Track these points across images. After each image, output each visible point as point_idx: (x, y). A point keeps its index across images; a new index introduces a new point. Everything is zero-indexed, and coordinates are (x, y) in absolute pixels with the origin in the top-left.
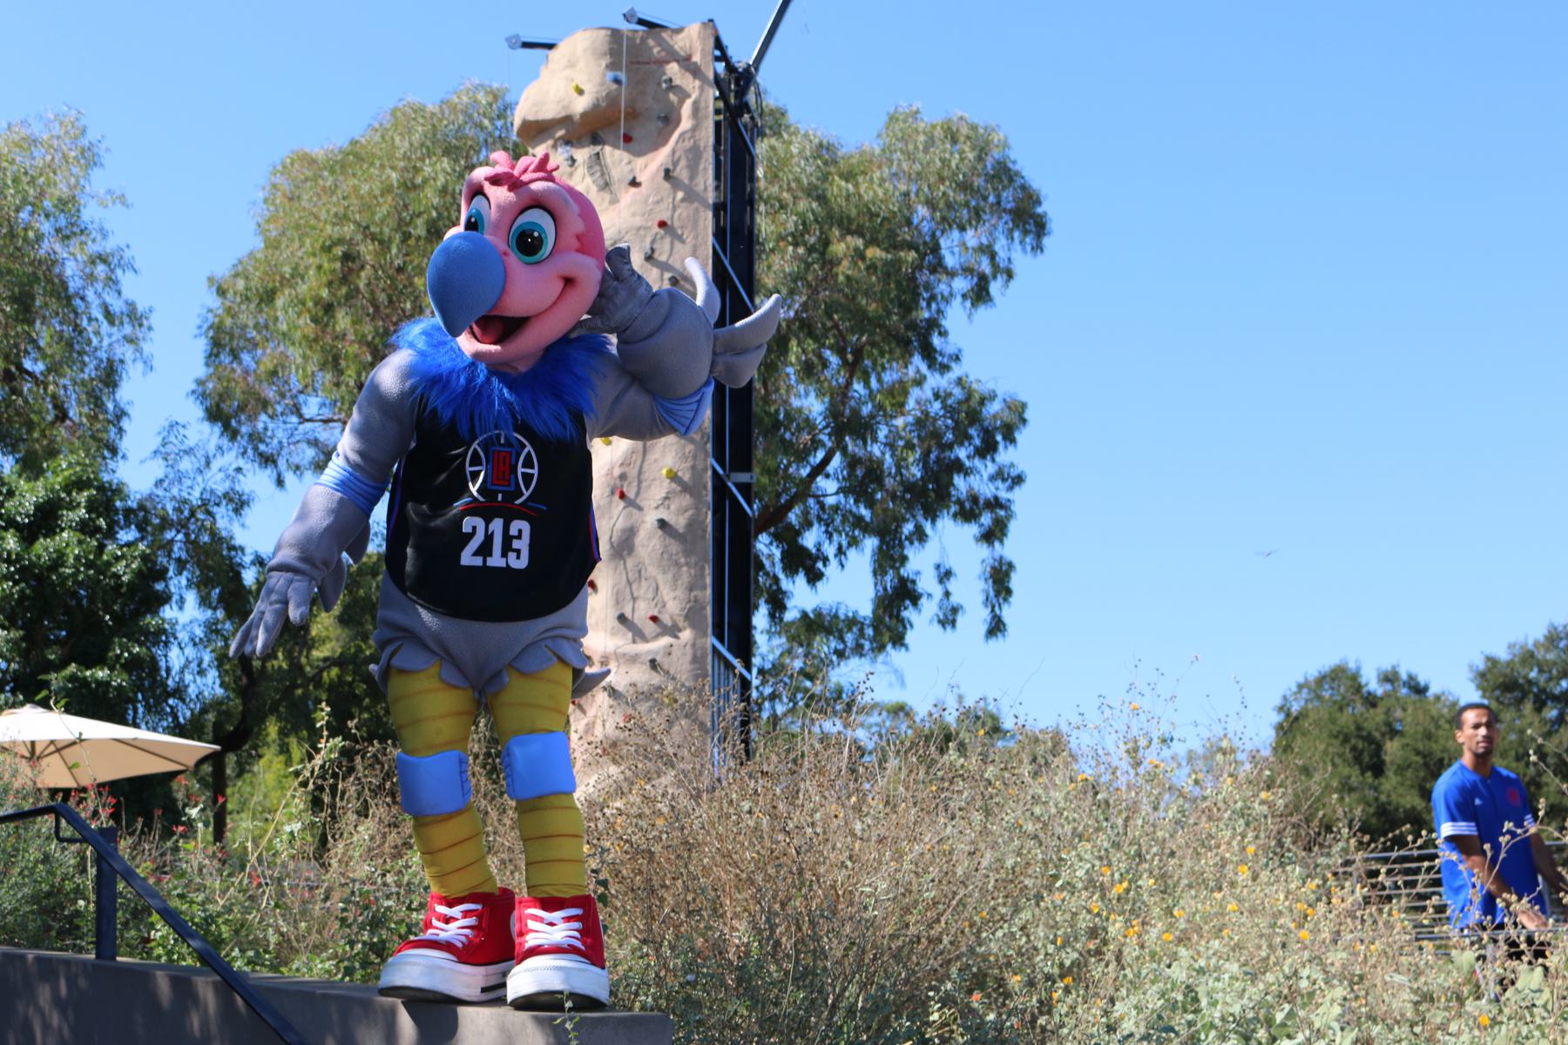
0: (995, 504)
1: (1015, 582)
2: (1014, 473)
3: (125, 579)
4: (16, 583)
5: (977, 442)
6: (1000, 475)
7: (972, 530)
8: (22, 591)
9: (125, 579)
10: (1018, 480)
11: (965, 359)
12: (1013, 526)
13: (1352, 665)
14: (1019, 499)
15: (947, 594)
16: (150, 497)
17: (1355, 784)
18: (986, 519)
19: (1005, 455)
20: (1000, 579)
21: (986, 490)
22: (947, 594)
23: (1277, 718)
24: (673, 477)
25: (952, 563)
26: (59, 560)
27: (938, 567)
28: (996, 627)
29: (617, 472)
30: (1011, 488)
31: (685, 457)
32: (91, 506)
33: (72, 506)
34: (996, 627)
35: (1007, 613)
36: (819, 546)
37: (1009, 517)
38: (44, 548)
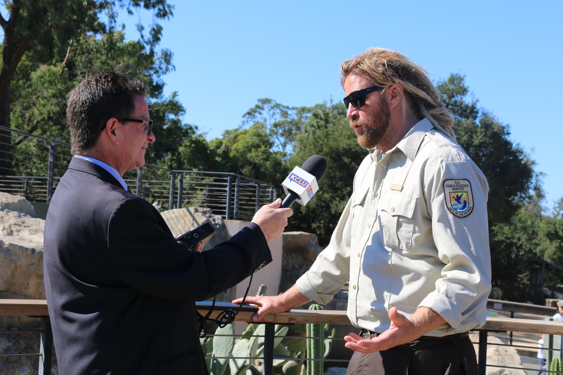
27: (138, 26)
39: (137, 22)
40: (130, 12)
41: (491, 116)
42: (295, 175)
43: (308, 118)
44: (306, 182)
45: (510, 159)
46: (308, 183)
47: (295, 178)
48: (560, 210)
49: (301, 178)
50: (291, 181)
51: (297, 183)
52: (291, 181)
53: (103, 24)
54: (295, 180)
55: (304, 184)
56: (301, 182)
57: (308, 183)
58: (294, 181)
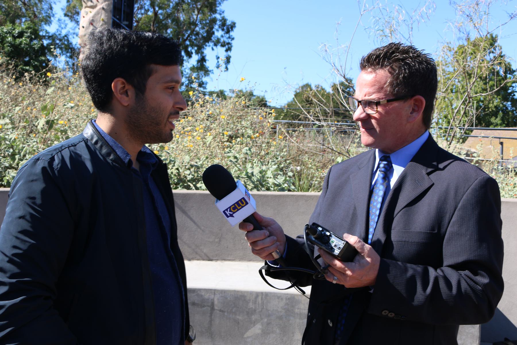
0: (229, 44)
1: (231, 60)
2: (232, 37)
3: (36, 49)
4: (10, 48)
5: (226, 30)
6: (229, 38)
7: (224, 49)
8: (11, 49)
9: (36, 49)
10: (233, 39)
11: (225, 13)
12: (233, 48)
13: (310, 84)
14: (233, 43)
15: (218, 62)
16: (55, 34)
17: (58, 49)
18: (227, 47)
19: (231, 33)
20: (228, 60)
21: (227, 41)
22: (218, 62)
23: (294, 93)
24: (103, 20)
25: (219, 56)
26: (21, 43)
27: (217, 56)
28: (227, 68)
29: (91, 19)
30: (231, 40)
31: (106, 16)
32: (31, 33)
33: (27, 33)
34: (227, 68)
35: (229, 66)
36: (191, 50)
37: (231, 47)
38: (18, 41)
39: (216, 54)
40: (213, 49)
41: (377, 191)
42: (227, 210)
43: (235, 92)
44: (240, 200)
45: (37, 62)
46: (243, 198)
47: (230, 211)
48: (345, 268)
49: (234, 204)
50: (233, 217)
51: (238, 210)
52: (233, 217)
53: (196, 54)
54: (234, 211)
55: (243, 203)
56: (239, 205)
57: (243, 198)
58: (234, 213)
